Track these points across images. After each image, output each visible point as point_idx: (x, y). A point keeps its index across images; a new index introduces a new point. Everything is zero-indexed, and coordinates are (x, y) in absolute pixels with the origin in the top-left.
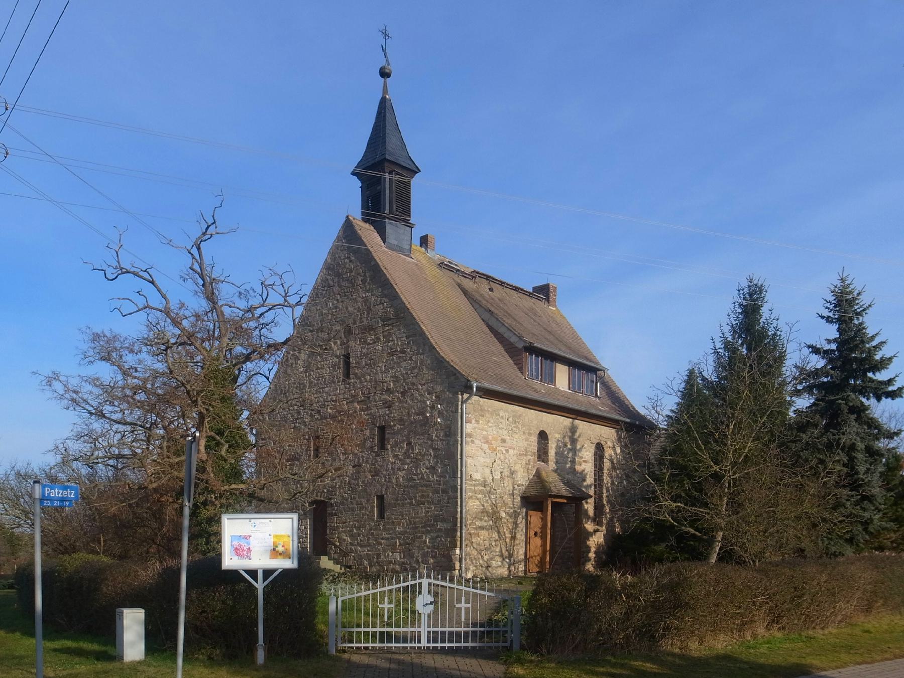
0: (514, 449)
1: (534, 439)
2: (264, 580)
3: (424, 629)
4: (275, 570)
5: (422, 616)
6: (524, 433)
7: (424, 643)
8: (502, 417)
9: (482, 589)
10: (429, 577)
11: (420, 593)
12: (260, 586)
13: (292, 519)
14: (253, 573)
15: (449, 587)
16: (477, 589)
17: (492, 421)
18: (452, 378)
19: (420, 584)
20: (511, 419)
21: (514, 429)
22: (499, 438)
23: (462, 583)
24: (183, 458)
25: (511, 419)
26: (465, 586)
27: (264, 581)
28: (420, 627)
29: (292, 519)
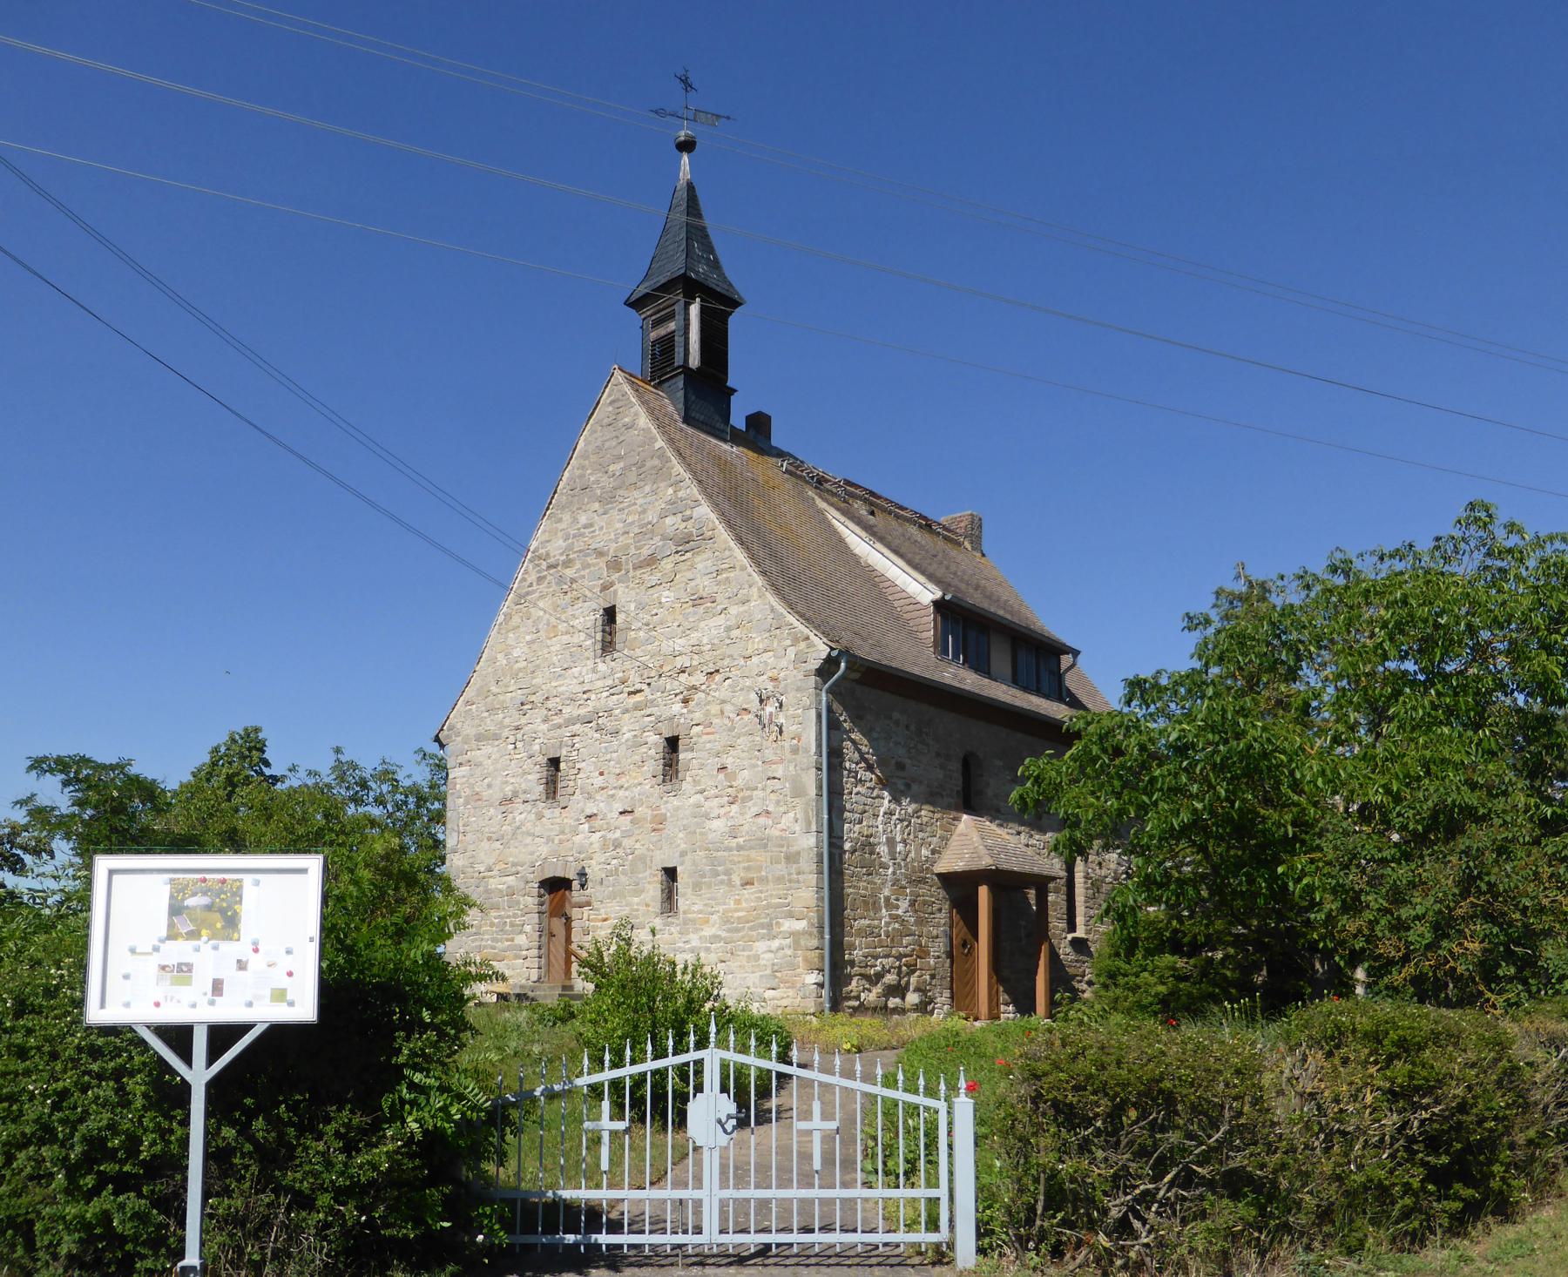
0: (921, 783)
1: (955, 766)
2: (212, 1057)
3: (711, 1195)
4: (244, 1028)
5: (706, 1154)
6: (938, 755)
7: (711, 1236)
8: (897, 723)
9: (848, 1074)
10: (722, 1044)
11: (699, 1088)
12: (198, 1075)
13: (111, 872)
14: (178, 1037)
15: (820, 1084)
16: (831, 1073)
17: (878, 729)
18: (803, 645)
19: (699, 1063)
20: (913, 728)
21: (919, 746)
22: (893, 762)
23: (896, 1081)
24: (672, 326)
25: (913, 728)
26: (905, 1090)
27: (210, 1062)
28: (723, 1204)
29: (111, 872)
